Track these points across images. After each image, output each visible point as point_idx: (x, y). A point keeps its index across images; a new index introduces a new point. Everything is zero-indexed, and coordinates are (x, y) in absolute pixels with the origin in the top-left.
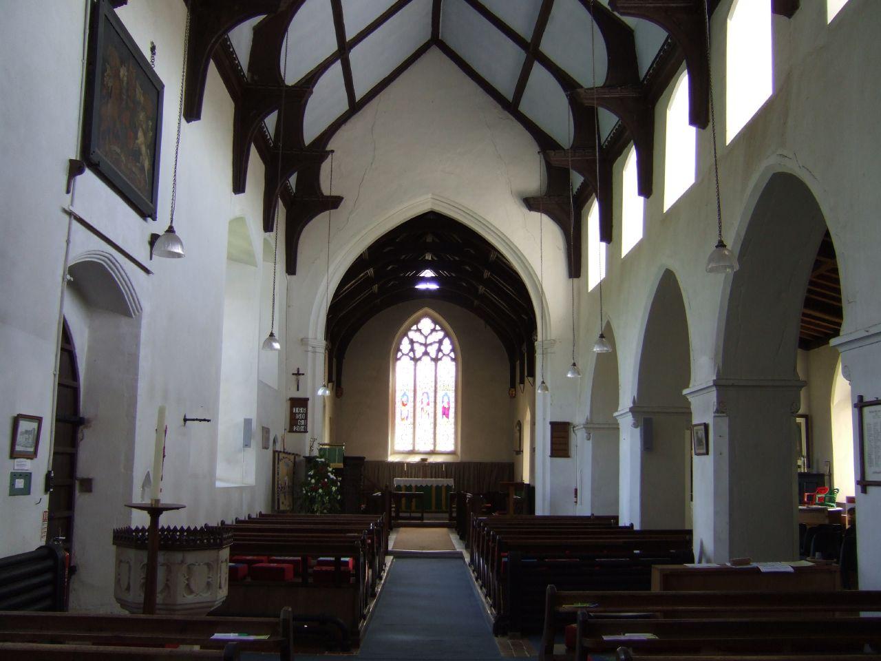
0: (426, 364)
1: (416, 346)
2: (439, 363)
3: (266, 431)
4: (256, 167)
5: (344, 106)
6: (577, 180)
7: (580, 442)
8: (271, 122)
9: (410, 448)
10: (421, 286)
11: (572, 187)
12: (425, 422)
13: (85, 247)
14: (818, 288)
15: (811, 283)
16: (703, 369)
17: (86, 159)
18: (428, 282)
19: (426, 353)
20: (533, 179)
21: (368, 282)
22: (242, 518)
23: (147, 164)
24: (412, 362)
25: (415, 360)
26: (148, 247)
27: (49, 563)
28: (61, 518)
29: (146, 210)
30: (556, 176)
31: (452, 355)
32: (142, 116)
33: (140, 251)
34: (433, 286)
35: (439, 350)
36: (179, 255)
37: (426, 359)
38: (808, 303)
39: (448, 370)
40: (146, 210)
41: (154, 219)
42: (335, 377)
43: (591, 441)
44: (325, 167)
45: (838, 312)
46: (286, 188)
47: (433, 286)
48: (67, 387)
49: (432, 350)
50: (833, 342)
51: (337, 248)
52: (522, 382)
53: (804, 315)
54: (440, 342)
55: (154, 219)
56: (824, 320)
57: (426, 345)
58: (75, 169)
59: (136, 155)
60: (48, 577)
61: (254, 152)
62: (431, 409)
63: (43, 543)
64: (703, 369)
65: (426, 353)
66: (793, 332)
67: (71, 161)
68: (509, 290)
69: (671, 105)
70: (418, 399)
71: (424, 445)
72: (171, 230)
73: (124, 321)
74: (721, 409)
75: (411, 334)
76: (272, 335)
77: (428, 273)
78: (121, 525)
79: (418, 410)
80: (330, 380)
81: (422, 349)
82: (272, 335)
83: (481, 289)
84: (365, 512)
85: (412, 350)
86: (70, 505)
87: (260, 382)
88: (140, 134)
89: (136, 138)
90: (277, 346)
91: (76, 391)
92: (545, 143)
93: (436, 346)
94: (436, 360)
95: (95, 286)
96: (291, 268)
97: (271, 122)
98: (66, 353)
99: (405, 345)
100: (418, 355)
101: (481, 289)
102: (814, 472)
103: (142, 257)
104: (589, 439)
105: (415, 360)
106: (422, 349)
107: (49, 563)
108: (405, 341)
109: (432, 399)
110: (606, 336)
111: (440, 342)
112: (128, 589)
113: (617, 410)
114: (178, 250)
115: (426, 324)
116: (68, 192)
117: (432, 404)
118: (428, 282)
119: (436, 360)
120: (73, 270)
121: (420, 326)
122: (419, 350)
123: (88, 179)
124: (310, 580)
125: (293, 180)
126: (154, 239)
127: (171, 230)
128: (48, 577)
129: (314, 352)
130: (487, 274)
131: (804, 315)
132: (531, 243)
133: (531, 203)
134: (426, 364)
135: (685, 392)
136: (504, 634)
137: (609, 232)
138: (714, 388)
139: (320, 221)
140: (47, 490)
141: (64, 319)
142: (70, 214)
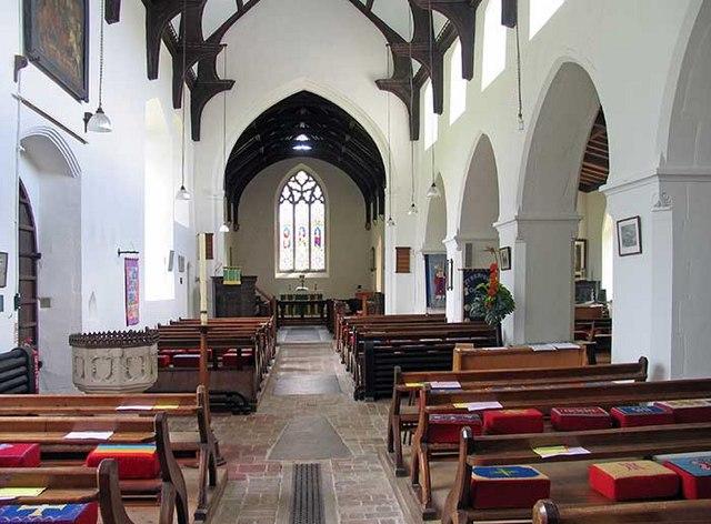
0: (302, 206)
1: (295, 193)
2: (312, 205)
3: (181, 259)
4: (165, 55)
5: (235, 10)
6: (416, 66)
7: (418, 264)
8: (176, 22)
9: (291, 268)
10: (298, 148)
11: (413, 70)
12: (302, 250)
13: (35, 124)
14: (60, 423)
15: (589, 143)
16: (508, 207)
17: (31, 54)
18: (302, 143)
19: (302, 198)
20: (383, 64)
21: (257, 145)
22: (175, 320)
23: (79, 59)
24: (291, 205)
25: (294, 203)
26: (83, 123)
27: (22, 359)
28: (29, 329)
29: (80, 94)
30: (401, 63)
31: (322, 199)
32: (72, 20)
33: (78, 128)
34: (307, 148)
35: (312, 195)
36: (108, 130)
37: (302, 202)
38: (587, 158)
39: (319, 209)
40: (80, 94)
41: (87, 102)
42: (232, 216)
43: (172, 273)
44: (220, 57)
45: (606, 164)
46: (190, 74)
47: (307, 148)
48: (24, 230)
49: (307, 196)
50: (601, 188)
51: (232, 117)
52: (375, 218)
53: (584, 166)
54: (313, 189)
55: (87, 102)
56: (599, 171)
57: (302, 192)
58: (20, 63)
59: (69, 51)
60: (22, 369)
61: (164, 50)
62: (306, 239)
63: (16, 346)
64: (508, 207)
65: (302, 198)
66: (575, 180)
67: (16, 57)
68: (365, 150)
69: (449, 95)
70: (297, 233)
71: (302, 265)
72: (100, 111)
73: (67, 179)
74: (520, 238)
75: (291, 184)
76: (183, 188)
77: (302, 138)
78: (76, 332)
79: (297, 240)
80: (229, 220)
81: (299, 195)
82: (183, 188)
83: (344, 149)
84: (258, 315)
85: (292, 195)
86: (34, 318)
87: (175, 224)
88: (71, 34)
89: (69, 38)
90: (187, 196)
91: (33, 234)
92: (392, 37)
93: (309, 192)
94: (310, 203)
95: (43, 151)
96: (196, 136)
97: (176, 22)
98: (23, 206)
99: (286, 193)
100: (296, 199)
101: (344, 149)
102: (589, 280)
103: (80, 131)
104: (170, 270)
105: (294, 203)
106: (299, 195)
107: (22, 359)
108: (286, 188)
109: (307, 231)
110: (437, 184)
111: (313, 189)
112: (83, 376)
113: (496, 221)
114: (106, 126)
115: (302, 176)
116: (16, 80)
117: (307, 235)
118: (302, 143)
119: (310, 203)
120: (23, 142)
121: (297, 178)
122: (297, 196)
123: (31, 69)
124: (220, 365)
125: (195, 68)
126: (88, 116)
127: (100, 111)
128: (22, 369)
129: (216, 199)
130: (348, 138)
131: (584, 166)
132: (380, 116)
133: (381, 85)
134: (302, 206)
135: (494, 224)
136: (362, 399)
137: (438, 107)
138: (657, 179)
139: (218, 99)
140: (16, 308)
141: (21, 182)
142: (18, 98)
